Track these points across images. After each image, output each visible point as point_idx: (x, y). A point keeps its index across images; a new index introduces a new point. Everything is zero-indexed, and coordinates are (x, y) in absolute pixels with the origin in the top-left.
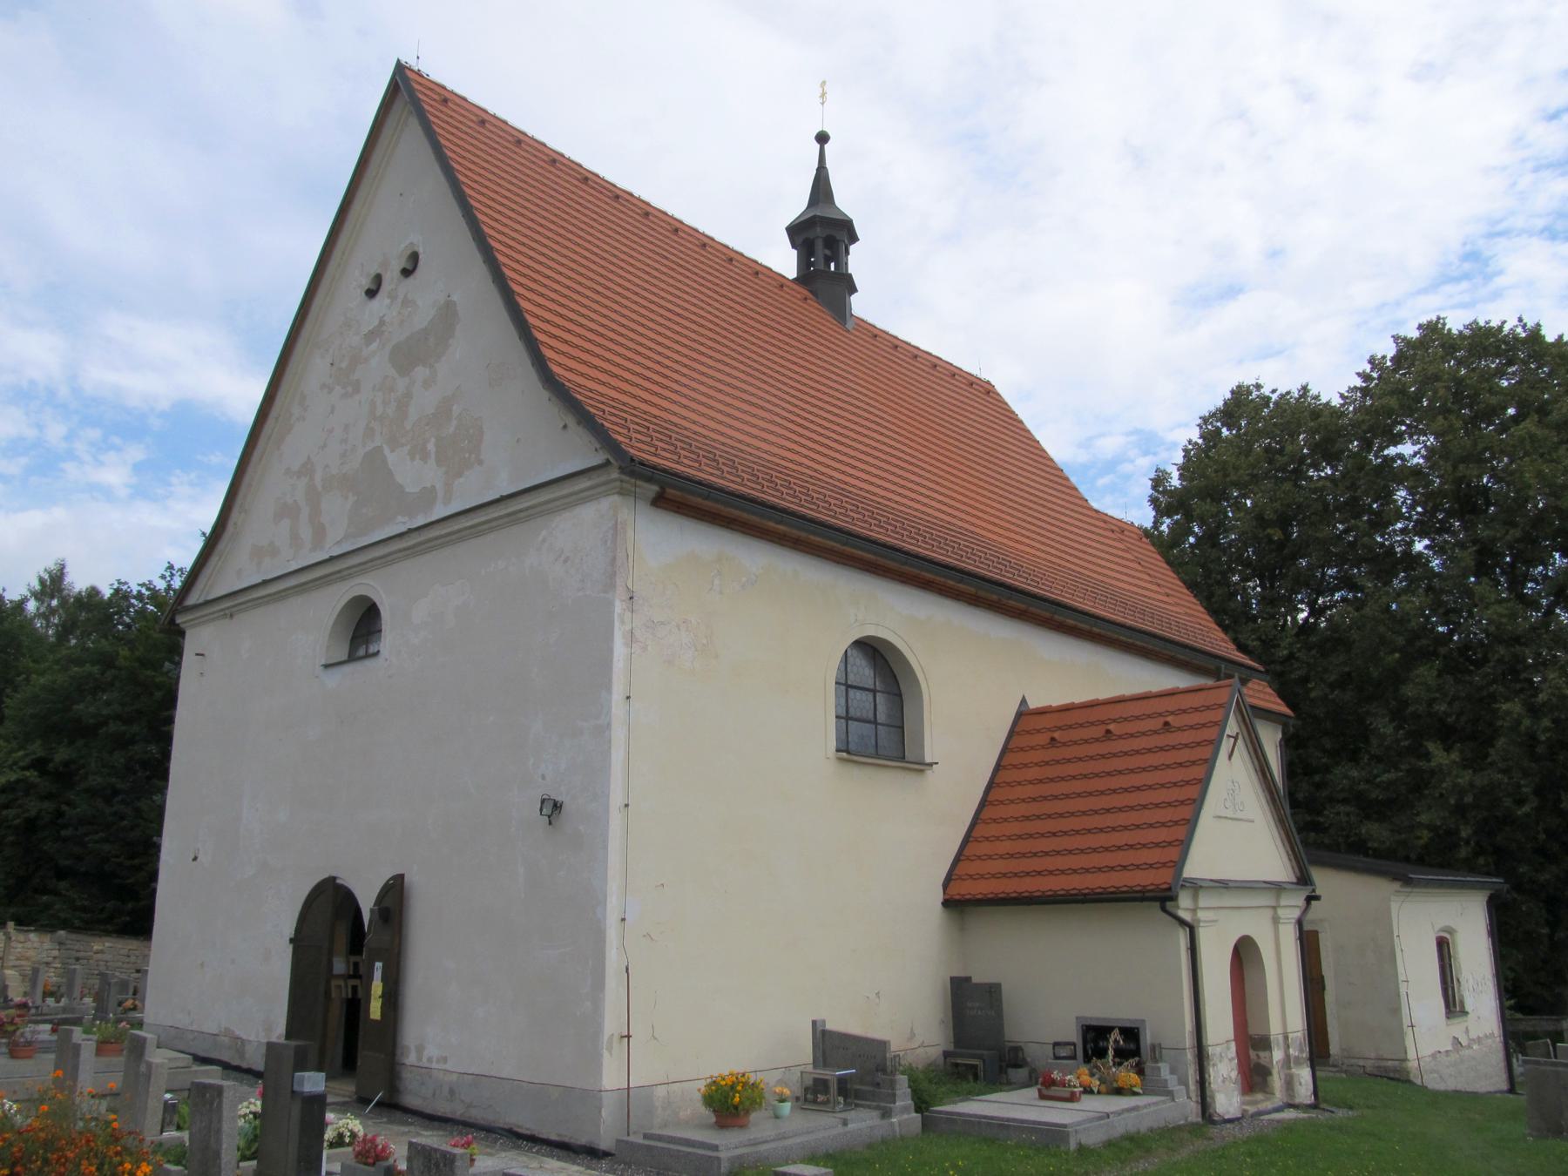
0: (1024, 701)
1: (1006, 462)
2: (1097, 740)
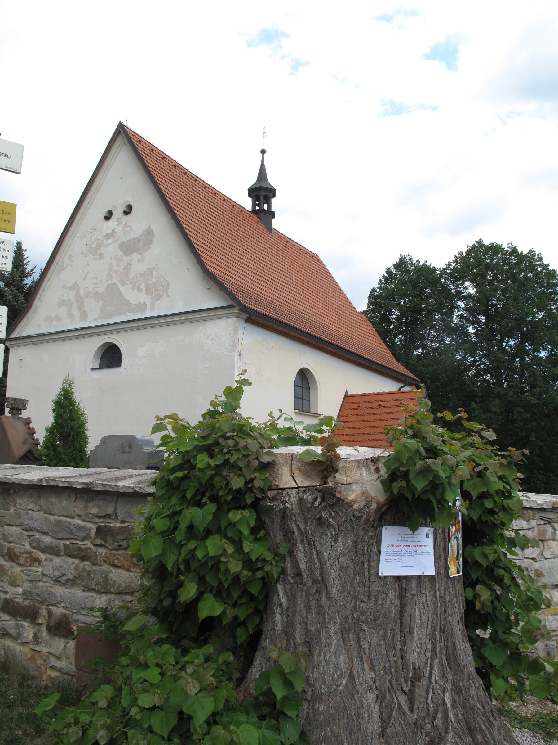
0: (347, 392)
2: (376, 408)
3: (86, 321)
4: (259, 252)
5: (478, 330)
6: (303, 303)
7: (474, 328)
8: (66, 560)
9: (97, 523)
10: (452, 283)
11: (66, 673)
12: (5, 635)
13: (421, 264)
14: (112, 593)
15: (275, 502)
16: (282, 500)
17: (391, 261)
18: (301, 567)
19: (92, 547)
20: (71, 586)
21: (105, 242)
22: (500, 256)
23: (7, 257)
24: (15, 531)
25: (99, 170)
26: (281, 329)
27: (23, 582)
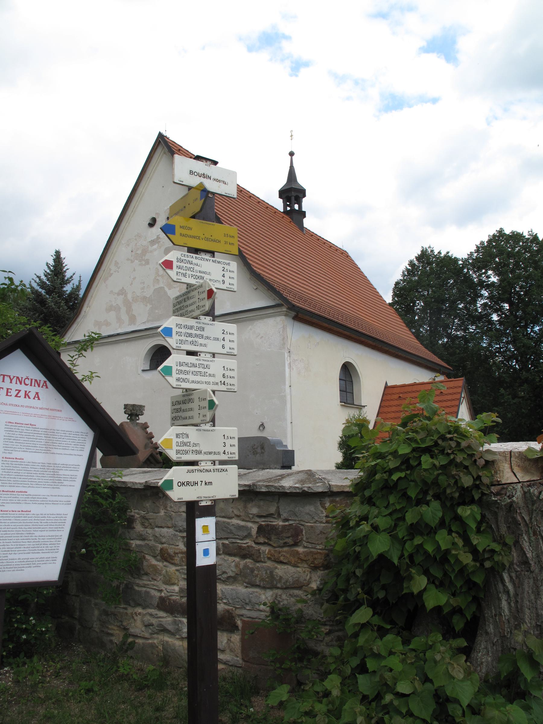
0: (386, 383)
1: (292, 246)
3: (135, 324)
4: (296, 251)
5: (501, 318)
6: (340, 299)
7: (498, 315)
8: (226, 558)
9: (257, 522)
10: (475, 272)
11: (232, 666)
12: (162, 631)
13: (442, 255)
14: (278, 588)
15: (499, 497)
16: (508, 494)
17: (414, 253)
18: (528, 555)
19: (254, 545)
20: (232, 583)
21: (150, 248)
22: (521, 244)
23: (233, 278)
24: (167, 532)
25: (141, 180)
26: (325, 325)
27: (178, 581)
